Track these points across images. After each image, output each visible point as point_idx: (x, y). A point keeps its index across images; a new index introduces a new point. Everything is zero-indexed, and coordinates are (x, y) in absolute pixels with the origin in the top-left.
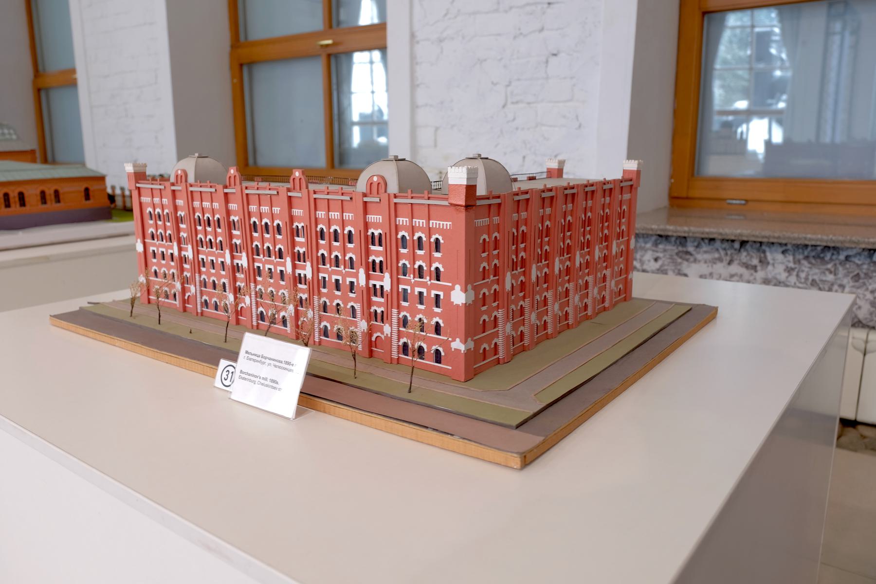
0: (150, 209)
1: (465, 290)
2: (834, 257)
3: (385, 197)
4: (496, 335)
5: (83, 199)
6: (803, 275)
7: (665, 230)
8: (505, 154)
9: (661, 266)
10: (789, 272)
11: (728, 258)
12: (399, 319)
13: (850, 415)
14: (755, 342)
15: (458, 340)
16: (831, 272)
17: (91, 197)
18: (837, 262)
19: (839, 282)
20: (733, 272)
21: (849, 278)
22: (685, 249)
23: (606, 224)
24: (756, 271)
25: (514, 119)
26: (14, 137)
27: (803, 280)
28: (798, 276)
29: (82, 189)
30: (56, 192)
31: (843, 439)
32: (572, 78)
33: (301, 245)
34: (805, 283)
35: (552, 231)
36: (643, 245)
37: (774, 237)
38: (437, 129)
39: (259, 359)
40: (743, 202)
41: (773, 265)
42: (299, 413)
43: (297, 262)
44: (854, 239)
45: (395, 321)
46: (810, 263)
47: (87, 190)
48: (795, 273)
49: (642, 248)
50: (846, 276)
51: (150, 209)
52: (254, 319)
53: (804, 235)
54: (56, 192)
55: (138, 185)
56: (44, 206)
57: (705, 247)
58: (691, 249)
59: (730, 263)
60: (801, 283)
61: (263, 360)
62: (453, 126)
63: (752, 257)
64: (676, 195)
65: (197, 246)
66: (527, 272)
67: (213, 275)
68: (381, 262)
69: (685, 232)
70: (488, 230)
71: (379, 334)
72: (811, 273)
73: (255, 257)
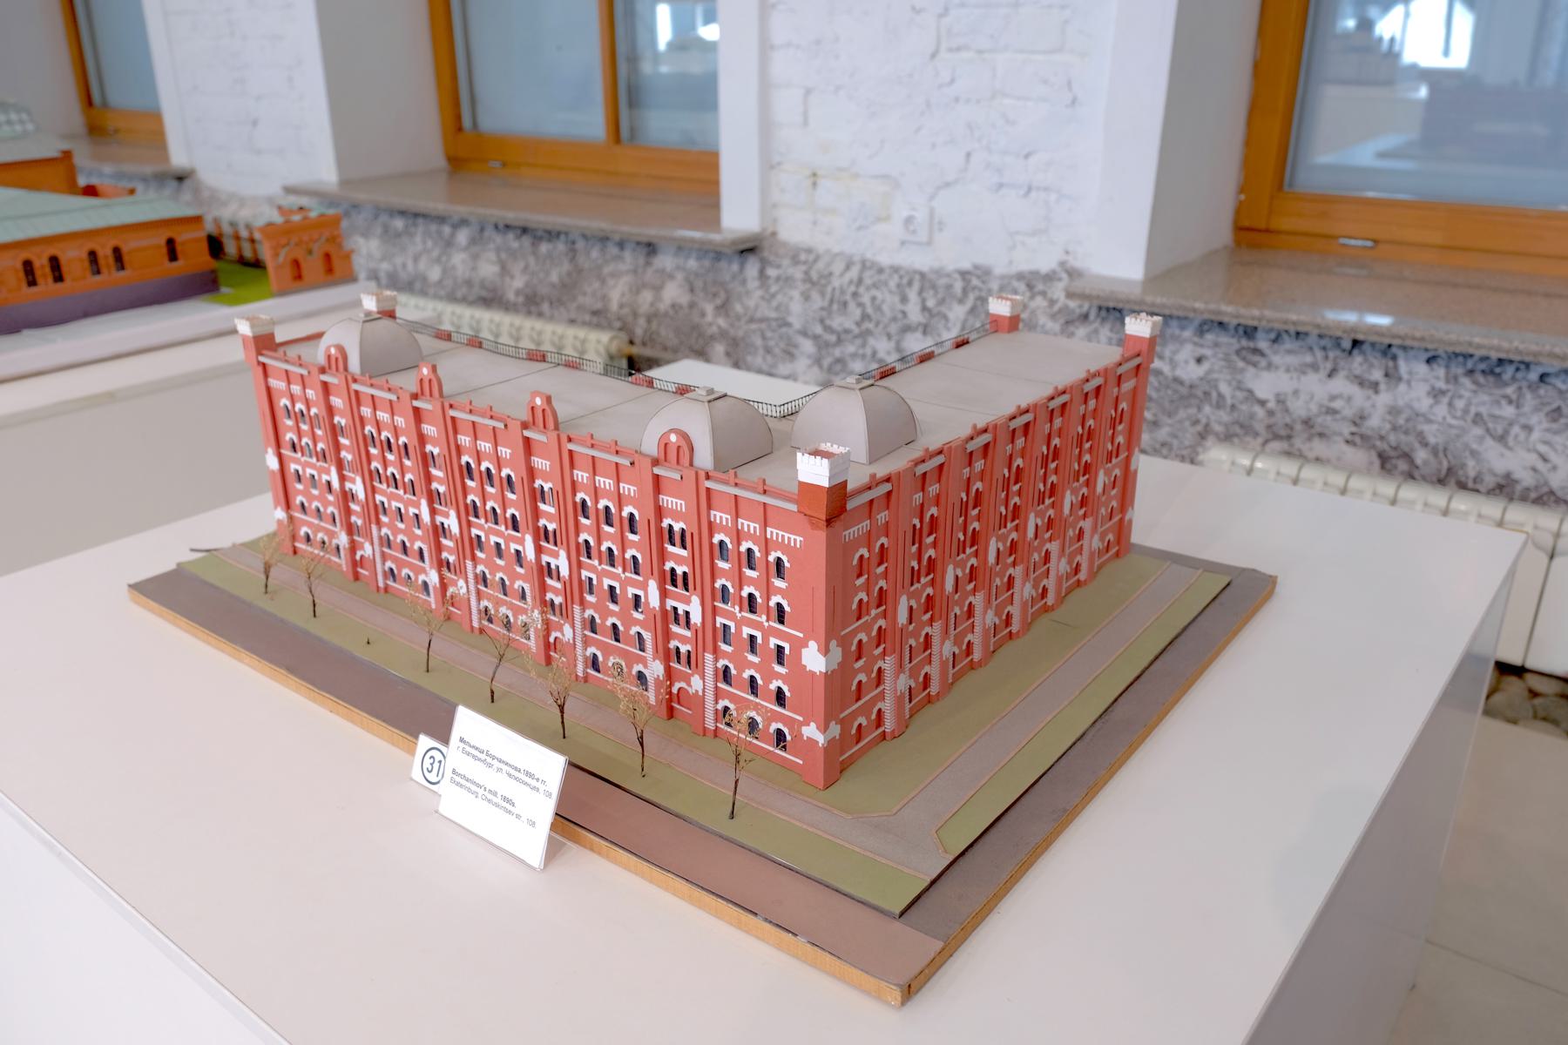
0: (285, 402)
1: (826, 651)
2: (1519, 375)
3: (690, 475)
4: (882, 696)
5: (166, 258)
6: (1460, 404)
7: (1219, 313)
8: (934, 146)
9: (1210, 372)
10: (1435, 396)
11: (1329, 366)
12: (716, 669)
13: (1514, 658)
14: (1349, 595)
15: (813, 725)
16: (1510, 402)
17: (180, 255)
18: (1524, 384)
19: (1523, 420)
20: (1335, 392)
21: (1542, 415)
22: (1251, 345)
23: (1087, 446)
24: (1377, 392)
25: (953, 81)
26: (30, 127)
27: (1459, 414)
28: (1450, 404)
29: (162, 241)
30: (117, 252)
31: (1497, 698)
32: (1063, 7)
33: (549, 517)
34: (1463, 418)
35: (985, 498)
36: (1177, 332)
37: (1414, 338)
38: (808, 92)
39: (483, 756)
40: (1369, 244)
41: (1409, 383)
42: (546, 865)
43: (544, 544)
44: (1557, 350)
45: (709, 671)
46: (1475, 382)
47: (171, 243)
48: (1445, 400)
49: (1175, 338)
50: (1537, 409)
51: (285, 402)
52: (475, 617)
53: (1467, 338)
54: (117, 252)
55: (262, 359)
56: (98, 278)
57: (1288, 344)
58: (1263, 344)
59: (1331, 374)
60: (1455, 417)
61: (489, 760)
62: (838, 88)
63: (1371, 366)
64: (1246, 224)
65: (372, 479)
66: (938, 580)
67: (401, 531)
68: (685, 573)
69: (1253, 318)
70: (868, 539)
71: (683, 685)
72: (1475, 401)
73: (472, 519)
